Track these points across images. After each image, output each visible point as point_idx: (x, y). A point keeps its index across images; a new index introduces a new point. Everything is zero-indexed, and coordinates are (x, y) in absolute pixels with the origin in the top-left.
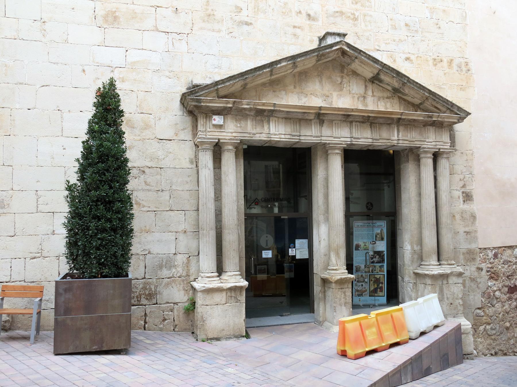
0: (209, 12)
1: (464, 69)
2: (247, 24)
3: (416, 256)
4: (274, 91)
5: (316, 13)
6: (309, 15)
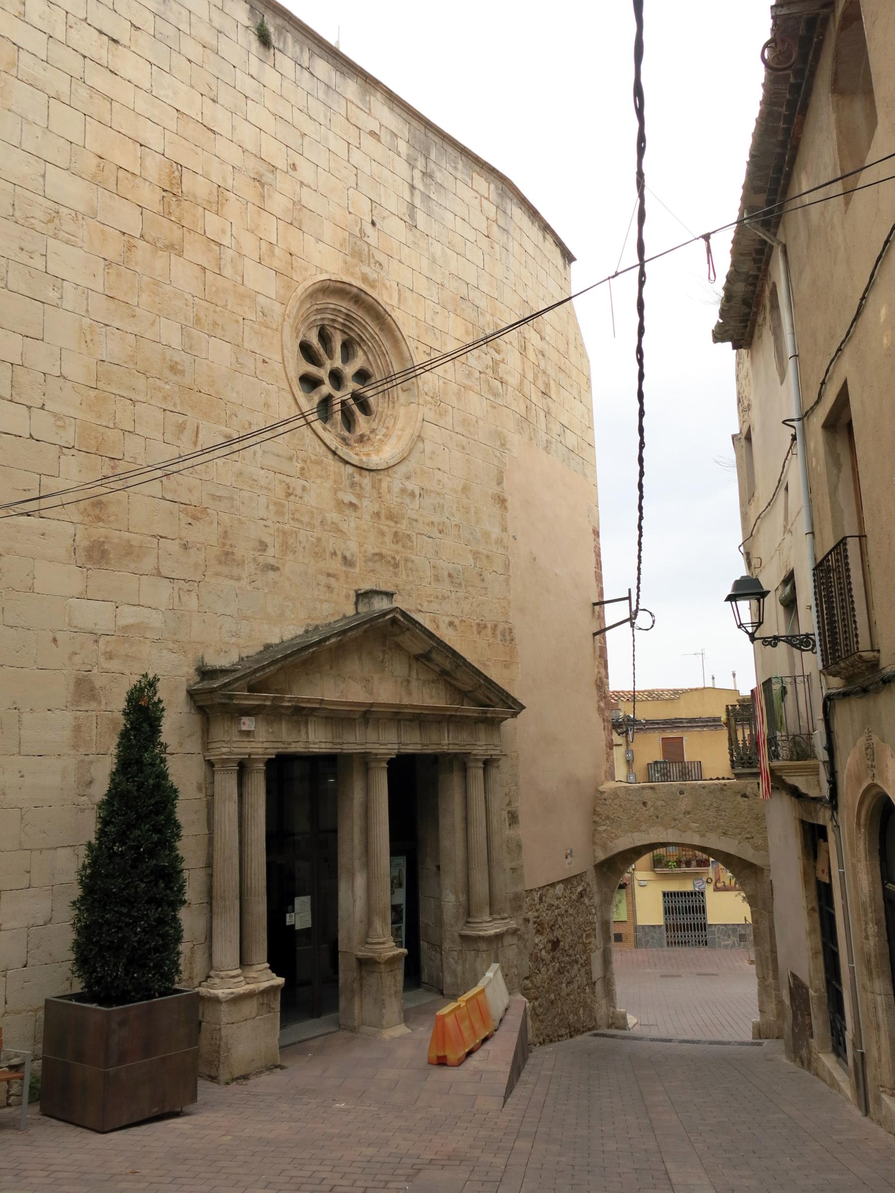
0: (227, 548)
1: (508, 638)
2: (274, 569)
3: (461, 911)
4: (307, 674)
5: (352, 555)
6: (345, 558)
